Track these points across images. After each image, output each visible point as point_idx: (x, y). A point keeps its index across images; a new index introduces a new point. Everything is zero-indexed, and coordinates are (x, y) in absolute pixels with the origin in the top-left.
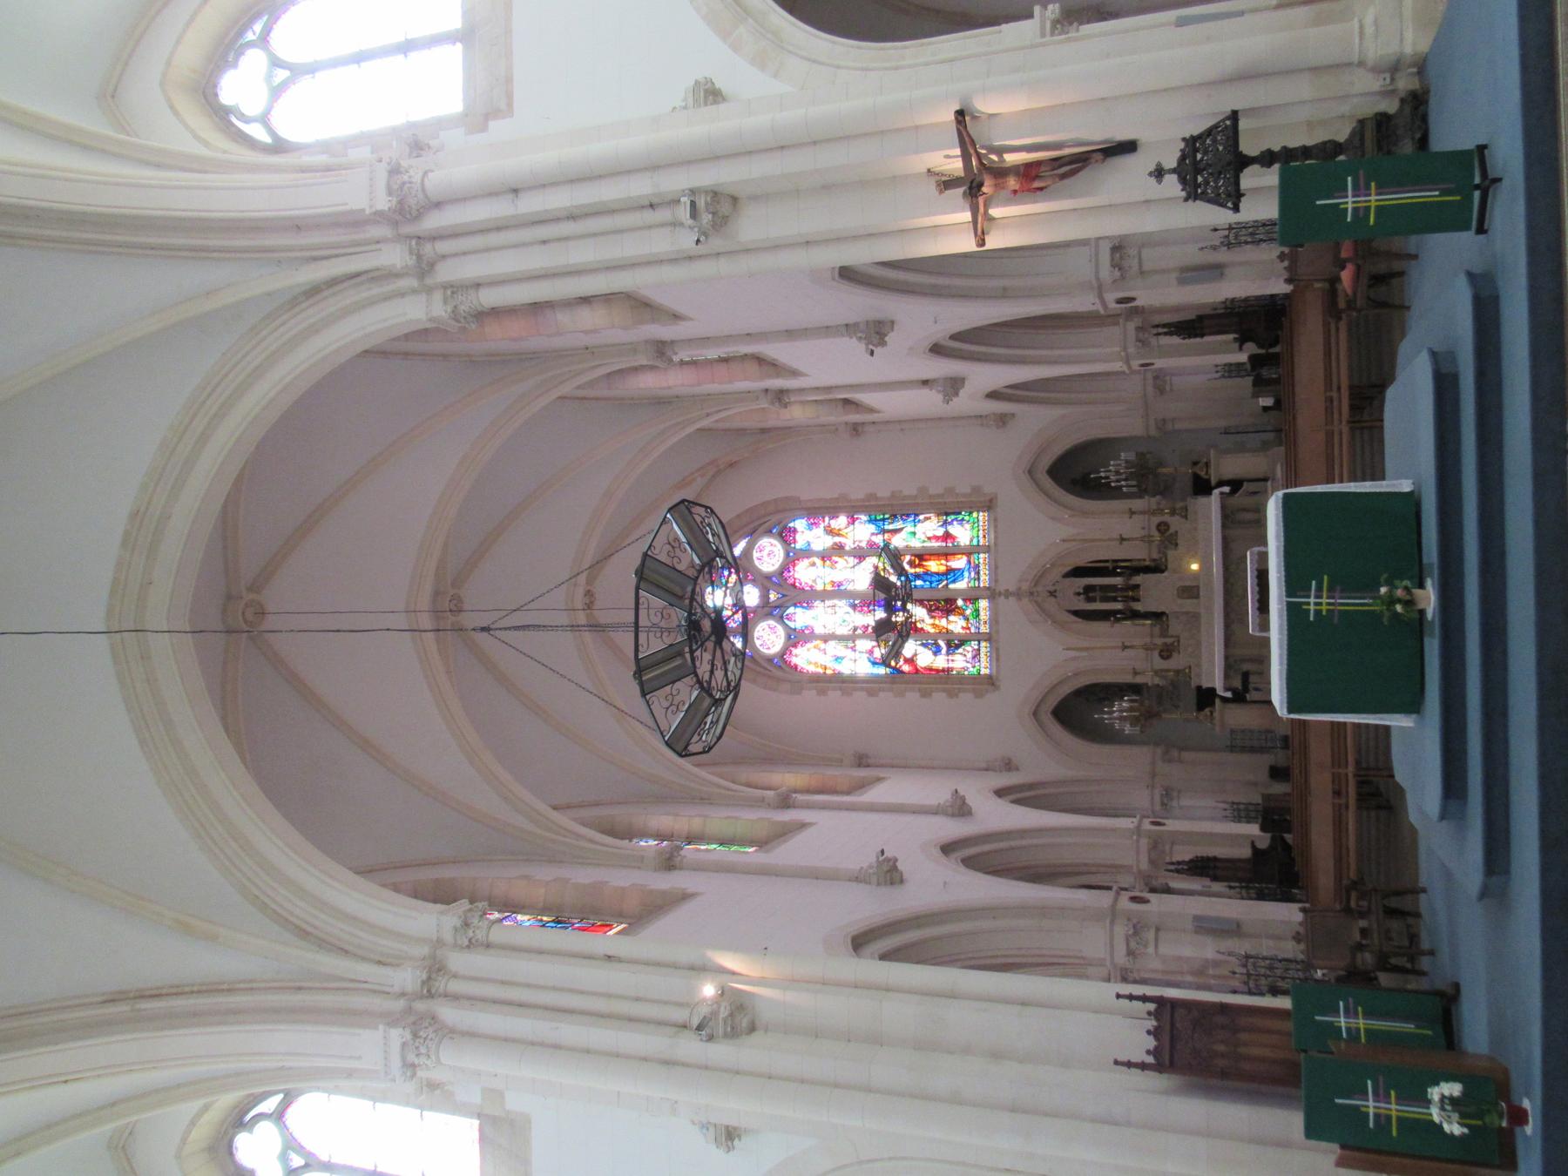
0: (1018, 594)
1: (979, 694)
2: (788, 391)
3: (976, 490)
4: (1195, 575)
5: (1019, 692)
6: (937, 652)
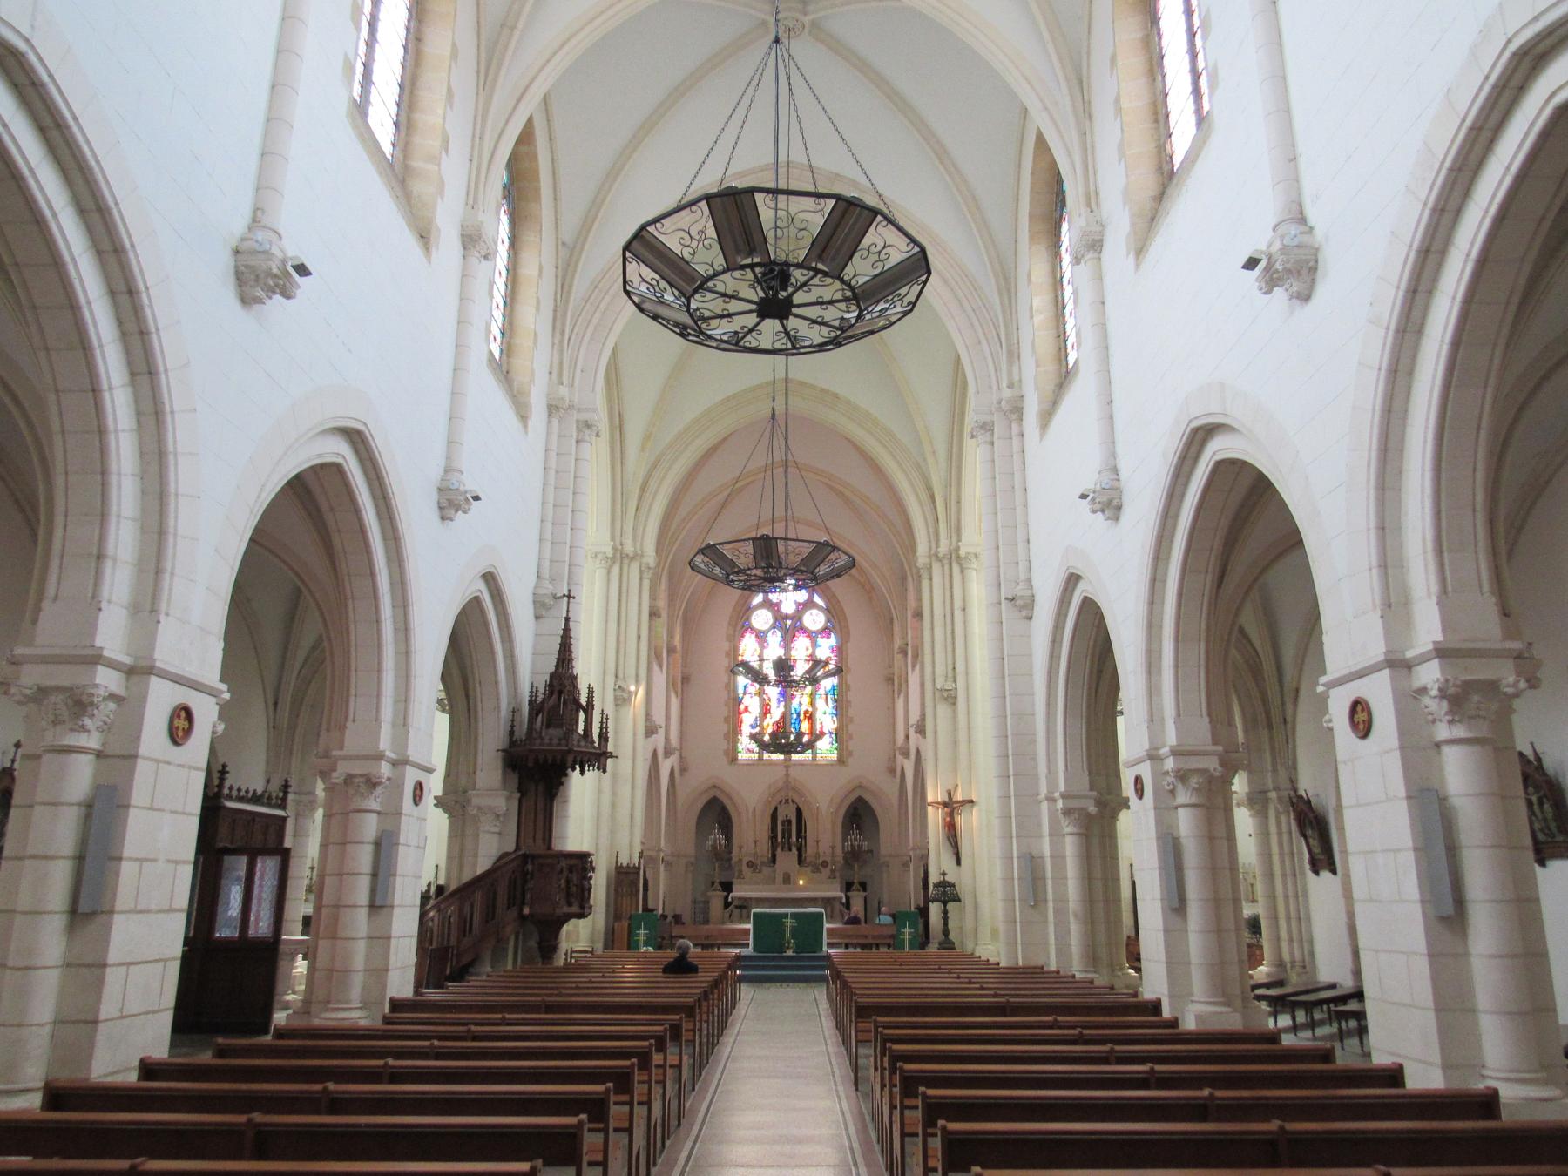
0: (787, 775)
1: (726, 752)
2: (1021, 419)
3: (850, 754)
4: (796, 883)
5: (730, 779)
6: (753, 727)
